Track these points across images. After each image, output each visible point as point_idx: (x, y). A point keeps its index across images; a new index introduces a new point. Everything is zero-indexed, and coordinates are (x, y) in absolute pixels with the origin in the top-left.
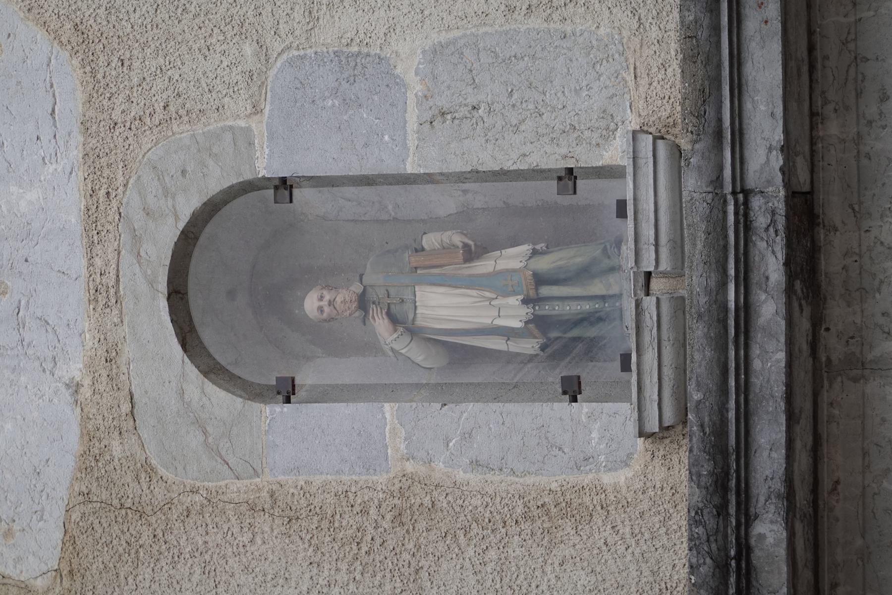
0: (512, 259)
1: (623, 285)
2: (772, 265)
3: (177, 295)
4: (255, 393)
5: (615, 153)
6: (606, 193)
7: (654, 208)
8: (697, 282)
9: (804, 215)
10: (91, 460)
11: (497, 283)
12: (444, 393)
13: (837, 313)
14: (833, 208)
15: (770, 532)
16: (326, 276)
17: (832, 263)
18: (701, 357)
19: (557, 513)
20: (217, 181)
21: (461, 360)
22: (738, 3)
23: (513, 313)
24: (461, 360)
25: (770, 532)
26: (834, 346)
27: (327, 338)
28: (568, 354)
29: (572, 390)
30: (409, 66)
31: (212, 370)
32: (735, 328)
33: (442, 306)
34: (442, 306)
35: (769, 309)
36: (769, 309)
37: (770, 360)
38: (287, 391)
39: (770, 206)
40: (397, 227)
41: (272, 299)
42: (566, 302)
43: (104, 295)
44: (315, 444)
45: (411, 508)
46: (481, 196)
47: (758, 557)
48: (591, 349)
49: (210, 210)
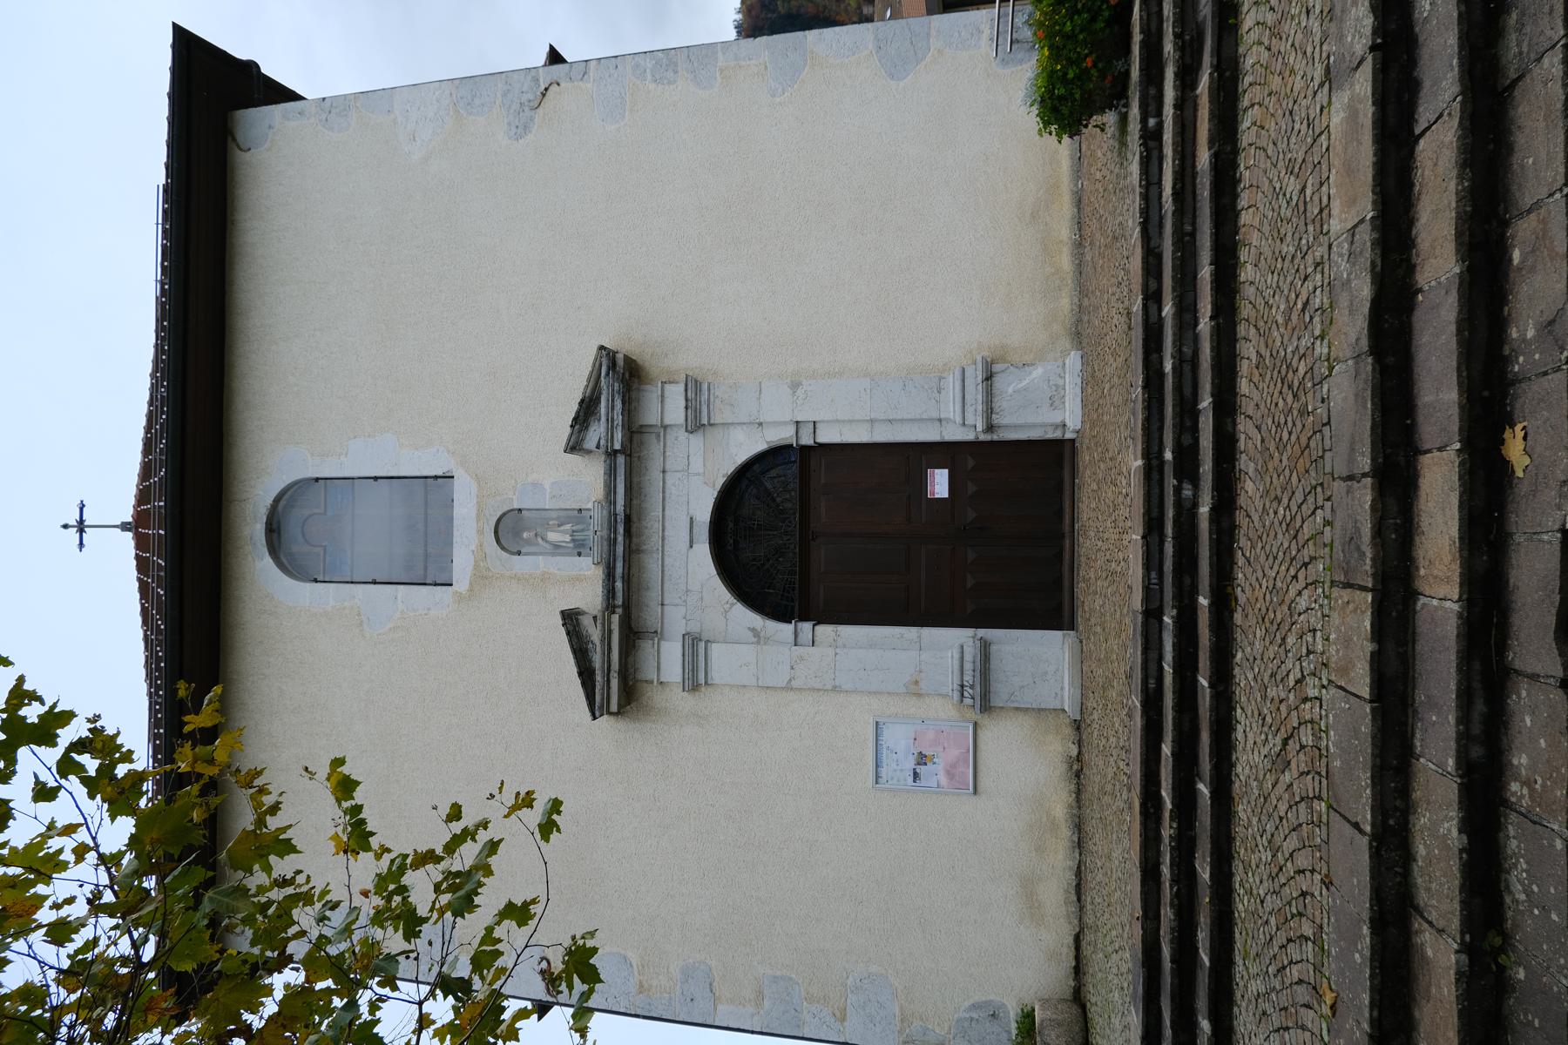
0: (568, 527)
1: (591, 533)
2: (621, 530)
3: (496, 532)
4: (513, 553)
5: (590, 506)
6: (588, 514)
7: (598, 518)
8: (605, 532)
9: (628, 520)
10: (476, 566)
11: (564, 532)
12: (553, 555)
13: (635, 540)
14: (634, 518)
15: (619, 585)
16: (528, 529)
17: (634, 529)
18: (606, 548)
19: (578, 579)
20: (506, 509)
21: (557, 548)
22: (1228, 11)
23: (568, 538)
24: (557, 548)
25: (619, 585)
26: (634, 547)
27: (528, 542)
28: (579, 548)
29: (579, 554)
30: (547, 486)
31: (503, 548)
32: (612, 543)
33: (553, 536)
34: (553, 536)
35: (620, 539)
36: (620, 539)
37: (620, 549)
38: (519, 553)
39: (621, 517)
40: (544, 520)
41: (517, 533)
42: (579, 536)
43: (480, 532)
44: (521, 564)
45: (545, 578)
46: (562, 513)
47: (1194, 175)
48: (583, 546)
49: (499, 521)
